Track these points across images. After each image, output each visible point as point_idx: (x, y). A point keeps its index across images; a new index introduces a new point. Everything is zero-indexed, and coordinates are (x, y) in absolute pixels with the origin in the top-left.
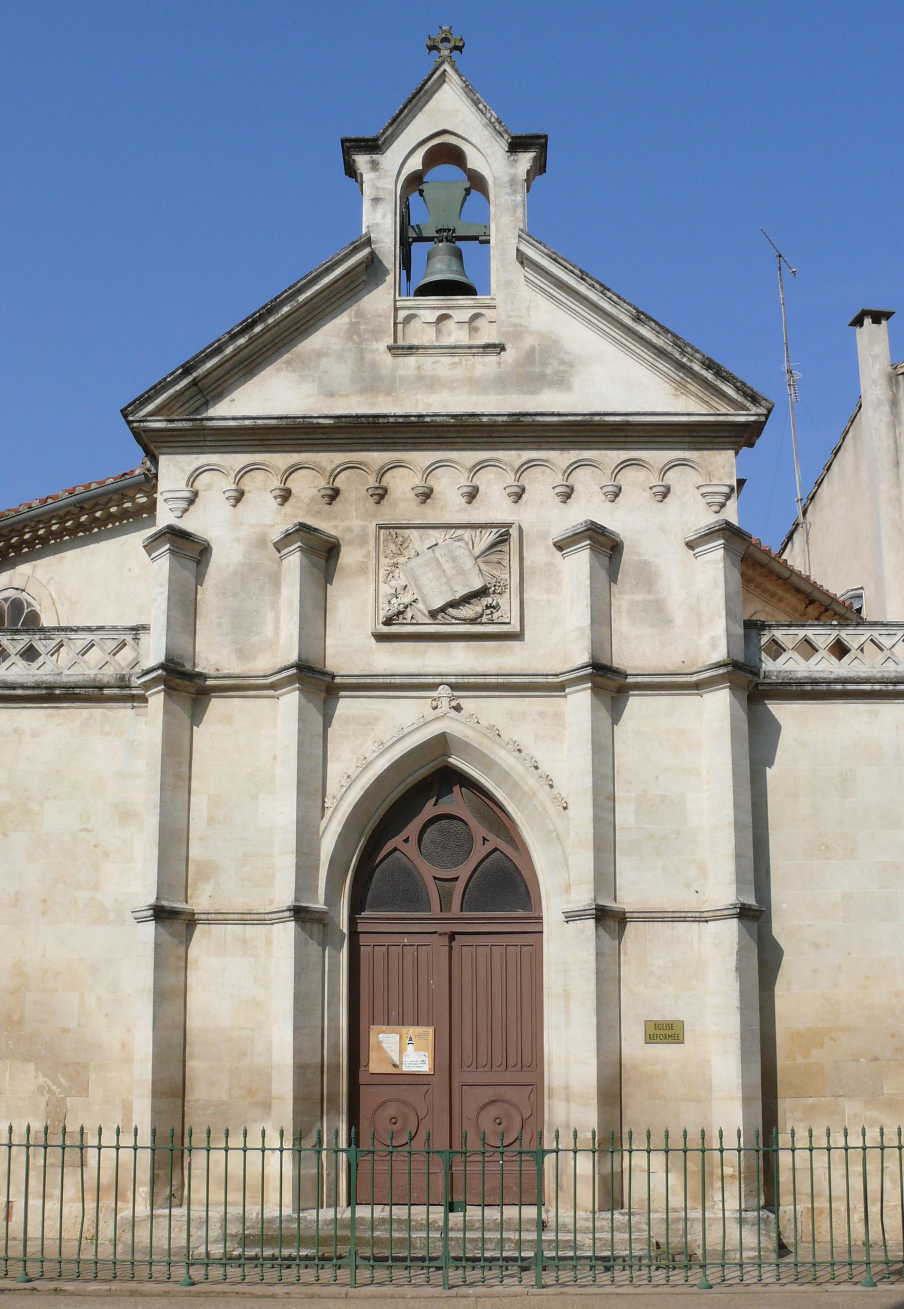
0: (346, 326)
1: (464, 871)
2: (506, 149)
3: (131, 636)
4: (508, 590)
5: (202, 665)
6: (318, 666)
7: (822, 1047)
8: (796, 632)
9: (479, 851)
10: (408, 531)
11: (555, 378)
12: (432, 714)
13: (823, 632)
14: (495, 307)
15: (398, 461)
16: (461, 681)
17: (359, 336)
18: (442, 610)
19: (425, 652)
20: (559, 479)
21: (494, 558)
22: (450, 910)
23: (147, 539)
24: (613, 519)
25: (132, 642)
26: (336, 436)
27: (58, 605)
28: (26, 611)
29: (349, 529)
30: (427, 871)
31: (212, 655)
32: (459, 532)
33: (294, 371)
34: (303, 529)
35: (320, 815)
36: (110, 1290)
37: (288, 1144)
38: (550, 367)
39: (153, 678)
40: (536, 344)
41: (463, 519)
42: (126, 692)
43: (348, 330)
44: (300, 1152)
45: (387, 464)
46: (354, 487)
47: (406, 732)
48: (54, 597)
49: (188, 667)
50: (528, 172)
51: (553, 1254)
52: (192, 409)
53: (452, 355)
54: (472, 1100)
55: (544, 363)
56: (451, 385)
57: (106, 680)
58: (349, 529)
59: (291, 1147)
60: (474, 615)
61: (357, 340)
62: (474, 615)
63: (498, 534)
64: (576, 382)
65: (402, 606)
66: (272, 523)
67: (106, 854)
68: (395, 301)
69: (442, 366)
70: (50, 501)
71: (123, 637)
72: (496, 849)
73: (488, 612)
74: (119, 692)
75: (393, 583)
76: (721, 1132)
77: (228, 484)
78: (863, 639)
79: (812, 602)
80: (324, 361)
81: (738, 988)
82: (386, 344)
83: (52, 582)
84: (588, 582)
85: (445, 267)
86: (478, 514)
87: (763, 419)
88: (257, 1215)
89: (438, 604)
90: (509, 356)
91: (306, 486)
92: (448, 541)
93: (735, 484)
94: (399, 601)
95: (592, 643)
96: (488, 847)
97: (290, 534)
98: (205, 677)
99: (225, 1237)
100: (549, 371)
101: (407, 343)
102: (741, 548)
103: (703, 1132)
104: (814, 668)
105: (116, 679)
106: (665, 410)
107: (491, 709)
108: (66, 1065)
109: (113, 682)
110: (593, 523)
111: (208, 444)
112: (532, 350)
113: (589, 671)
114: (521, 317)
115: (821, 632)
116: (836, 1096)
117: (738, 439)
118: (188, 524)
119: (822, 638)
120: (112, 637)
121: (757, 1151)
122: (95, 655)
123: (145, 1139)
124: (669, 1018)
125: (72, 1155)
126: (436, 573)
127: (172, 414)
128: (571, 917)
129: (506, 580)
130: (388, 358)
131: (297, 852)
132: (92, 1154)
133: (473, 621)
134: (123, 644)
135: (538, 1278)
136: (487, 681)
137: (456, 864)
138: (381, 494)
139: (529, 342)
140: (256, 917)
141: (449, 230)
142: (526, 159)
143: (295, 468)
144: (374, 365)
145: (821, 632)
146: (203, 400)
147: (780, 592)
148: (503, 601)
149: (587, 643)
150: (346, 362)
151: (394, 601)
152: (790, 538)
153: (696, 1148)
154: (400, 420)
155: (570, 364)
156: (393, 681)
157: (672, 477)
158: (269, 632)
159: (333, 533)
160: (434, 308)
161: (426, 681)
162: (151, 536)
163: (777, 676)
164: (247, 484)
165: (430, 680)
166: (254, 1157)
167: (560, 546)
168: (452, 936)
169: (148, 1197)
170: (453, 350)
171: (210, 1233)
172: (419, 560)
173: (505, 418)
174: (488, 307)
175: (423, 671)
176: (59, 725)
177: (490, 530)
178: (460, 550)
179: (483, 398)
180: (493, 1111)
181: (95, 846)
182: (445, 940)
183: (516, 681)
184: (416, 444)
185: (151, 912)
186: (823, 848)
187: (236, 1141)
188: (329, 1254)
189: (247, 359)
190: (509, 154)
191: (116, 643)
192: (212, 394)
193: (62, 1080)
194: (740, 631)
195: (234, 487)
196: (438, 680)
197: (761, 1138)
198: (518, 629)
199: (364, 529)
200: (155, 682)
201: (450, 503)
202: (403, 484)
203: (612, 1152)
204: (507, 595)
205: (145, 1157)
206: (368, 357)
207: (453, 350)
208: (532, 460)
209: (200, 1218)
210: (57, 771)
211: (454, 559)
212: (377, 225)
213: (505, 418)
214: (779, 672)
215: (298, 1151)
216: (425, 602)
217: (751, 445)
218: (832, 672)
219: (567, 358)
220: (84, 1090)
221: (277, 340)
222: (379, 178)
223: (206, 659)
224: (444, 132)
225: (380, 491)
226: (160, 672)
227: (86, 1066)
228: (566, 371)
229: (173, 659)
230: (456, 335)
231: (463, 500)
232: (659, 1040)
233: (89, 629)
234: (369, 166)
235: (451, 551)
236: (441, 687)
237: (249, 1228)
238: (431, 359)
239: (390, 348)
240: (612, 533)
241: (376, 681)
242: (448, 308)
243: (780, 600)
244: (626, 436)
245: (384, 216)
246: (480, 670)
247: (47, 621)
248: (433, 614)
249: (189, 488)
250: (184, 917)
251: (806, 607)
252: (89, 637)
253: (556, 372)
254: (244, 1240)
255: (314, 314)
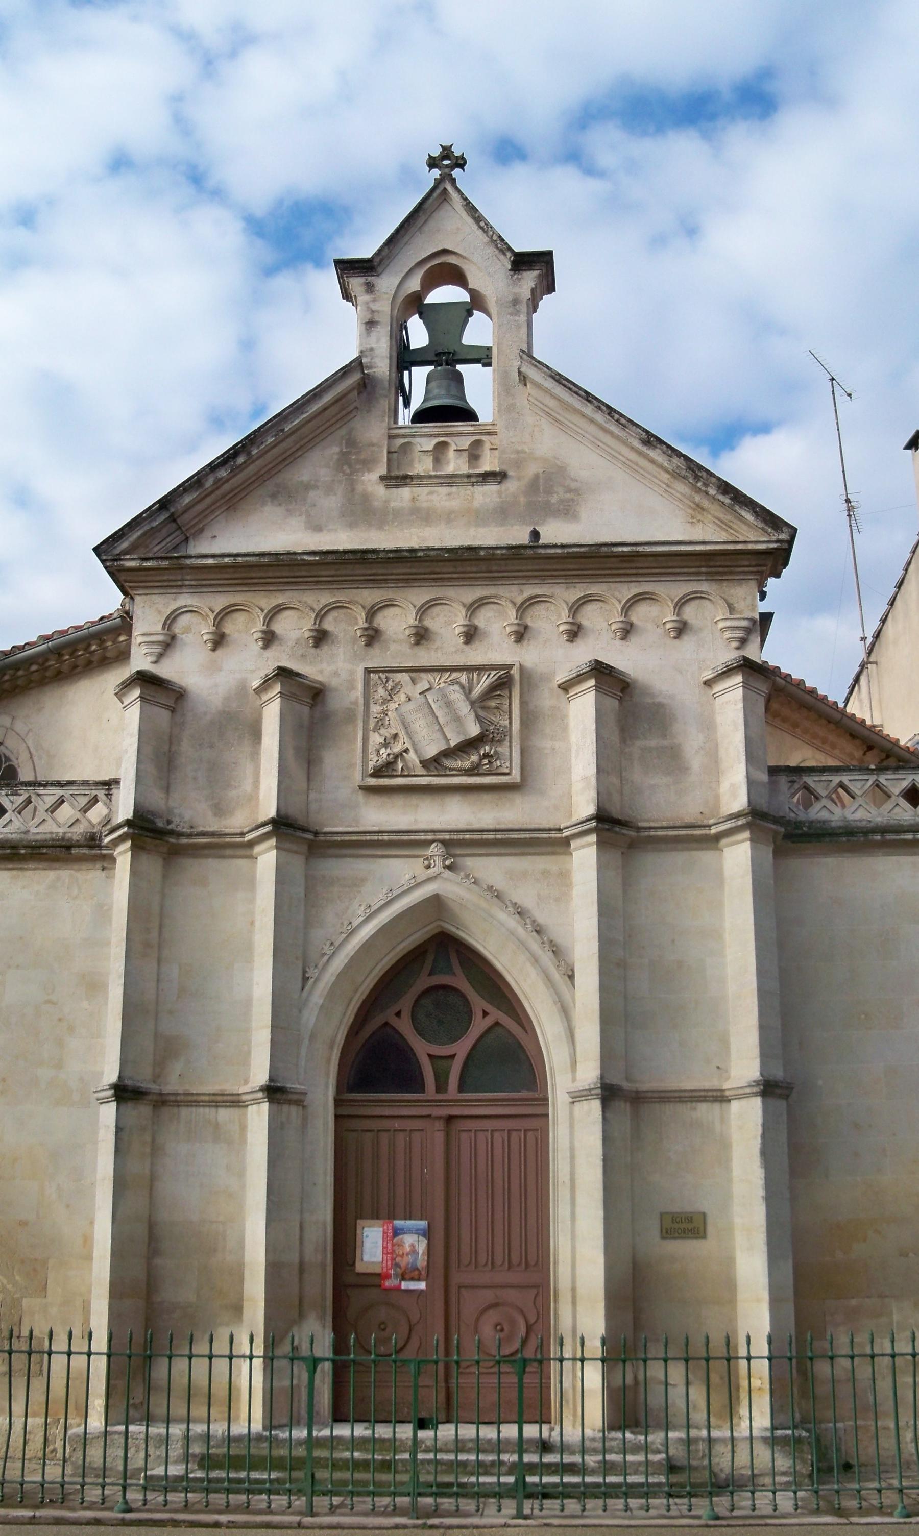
0: (336, 457)
1: (461, 1048)
2: (510, 267)
3: (103, 792)
4: (508, 738)
5: (175, 823)
6: (301, 821)
7: (865, 1240)
8: (830, 778)
9: (479, 1025)
10: (399, 675)
11: (561, 507)
12: (423, 874)
13: (861, 777)
14: (495, 433)
15: (390, 600)
16: (455, 837)
17: (350, 466)
18: (436, 760)
19: (417, 806)
20: (565, 615)
21: (493, 703)
22: (446, 1091)
23: (118, 686)
24: (624, 658)
25: (104, 798)
26: (323, 573)
27: (35, 759)
28: (3, 766)
29: (336, 674)
30: (422, 1048)
31: (192, 811)
32: (455, 675)
33: (280, 505)
34: (283, 673)
35: (300, 985)
36: (34, 1516)
37: (259, 1350)
38: (555, 495)
39: (120, 836)
40: (541, 471)
41: (460, 661)
42: (96, 852)
43: (339, 460)
44: (272, 1360)
45: (378, 603)
46: (346, 628)
47: (395, 893)
48: (32, 750)
49: (160, 824)
50: (533, 290)
51: (431, 1478)
52: (170, 546)
53: (450, 485)
54: (471, 1303)
55: (549, 492)
56: (449, 517)
57: (75, 838)
58: (336, 674)
59: (262, 1354)
60: (473, 762)
61: (348, 471)
62: (473, 762)
63: (496, 677)
64: (584, 513)
65: (391, 756)
66: (253, 668)
67: (71, 1029)
68: (390, 429)
69: (439, 498)
70: (27, 647)
71: (94, 793)
72: (497, 1024)
73: (486, 761)
74: (87, 850)
75: (382, 731)
76: (748, 1338)
77: (206, 629)
78: (833, 784)
79: (870, 748)
80: (312, 494)
81: (763, 1176)
82: (378, 475)
83: (30, 734)
84: (594, 727)
85: (443, 392)
86: (477, 655)
87: (785, 546)
88: (223, 1433)
89: (431, 751)
90: (511, 486)
91: (294, 627)
92: (442, 685)
93: (757, 617)
94: (389, 751)
95: (598, 794)
96: (489, 1021)
97: (269, 679)
98: (180, 835)
99: (187, 1458)
100: (554, 499)
101: (401, 473)
102: (764, 688)
103: (728, 1338)
104: (850, 817)
105: (86, 839)
106: (680, 538)
107: (491, 869)
108: (23, 1262)
109: (83, 842)
110: (597, 661)
111: (187, 583)
112: (537, 477)
113: (594, 824)
114: (525, 443)
115: (857, 777)
116: (882, 1296)
117: (760, 569)
118: (165, 670)
119: (859, 785)
120: (83, 792)
121: (790, 1359)
122: (66, 812)
123: (100, 1343)
124: (689, 1209)
125: (718, 1367)
126: (426, 723)
127: (148, 552)
128: (577, 1097)
129: (505, 727)
130: (380, 491)
131: (272, 1026)
132: (58, 1363)
133: (469, 772)
134: (95, 800)
135: (520, 1508)
136: (484, 837)
137: (454, 1039)
138: (372, 636)
139: (532, 469)
140: (229, 1098)
141: (449, 353)
142: (530, 279)
143: (278, 610)
144: (366, 498)
145: (857, 777)
146: (182, 537)
147: (832, 738)
148: (503, 749)
149: (593, 794)
150: (335, 494)
151: (383, 751)
152: (857, 680)
153: (720, 1355)
154: (391, 555)
155: (577, 491)
156: (380, 838)
157: (690, 612)
158: (248, 787)
159: (320, 678)
160: (431, 435)
161: (417, 838)
162: (123, 683)
163: (809, 828)
164: (229, 627)
165: (423, 837)
166: (221, 1365)
167: (565, 687)
168: (450, 1119)
169: (103, 1410)
170: (451, 480)
171: (171, 1453)
172: (411, 706)
173: (504, 551)
174: (490, 434)
175: (414, 827)
176: (24, 888)
177: (488, 673)
178: (456, 695)
179: (482, 530)
180: (492, 1317)
181: (60, 1020)
182: (440, 1125)
183: (516, 836)
184: (408, 581)
185: (112, 1092)
186: (863, 1016)
187: (201, 1348)
188: (303, 1475)
189: (229, 493)
190: (512, 273)
191: (87, 799)
192: (193, 531)
193: (17, 1278)
194: (764, 777)
195: (212, 629)
196: (430, 837)
197: (794, 1345)
198: (518, 780)
199: (352, 673)
200: (122, 839)
201: (447, 647)
202: (397, 623)
203: (624, 1362)
204: (507, 743)
205: (100, 1365)
206: (359, 488)
207: (451, 480)
208: (536, 597)
209: (159, 1435)
210: (21, 938)
211: (449, 704)
212: (372, 349)
213: (504, 551)
214: (812, 822)
215: (269, 1359)
216: (416, 751)
217: (778, 576)
218: (870, 821)
219: (573, 485)
220: (43, 1289)
221: (262, 472)
222: (374, 300)
223: (180, 815)
224: (445, 252)
225: (370, 632)
226: (126, 829)
227: (45, 1263)
228: (573, 500)
229: (142, 816)
230: (455, 464)
231: (461, 640)
232: (676, 1235)
233: (59, 784)
234: (363, 289)
235: (444, 696)
236: (434, 845)
237: (213, 1447)
238: (426, 490)
239: (382, 478)
240: (621, 673)
241: (364, 838)
242: (447, 435)
243: (833, 746)
244: (636, 568)
245: (378, 340)
246: (476, 826)
247: (25, 775)
248: (425, 764)
249: (166, 631)
250: (150, 1097)
251: (864, 754)
252: (59, 792)
253: (561, 501)
254: (207, 1462)
255: (302, 443)
